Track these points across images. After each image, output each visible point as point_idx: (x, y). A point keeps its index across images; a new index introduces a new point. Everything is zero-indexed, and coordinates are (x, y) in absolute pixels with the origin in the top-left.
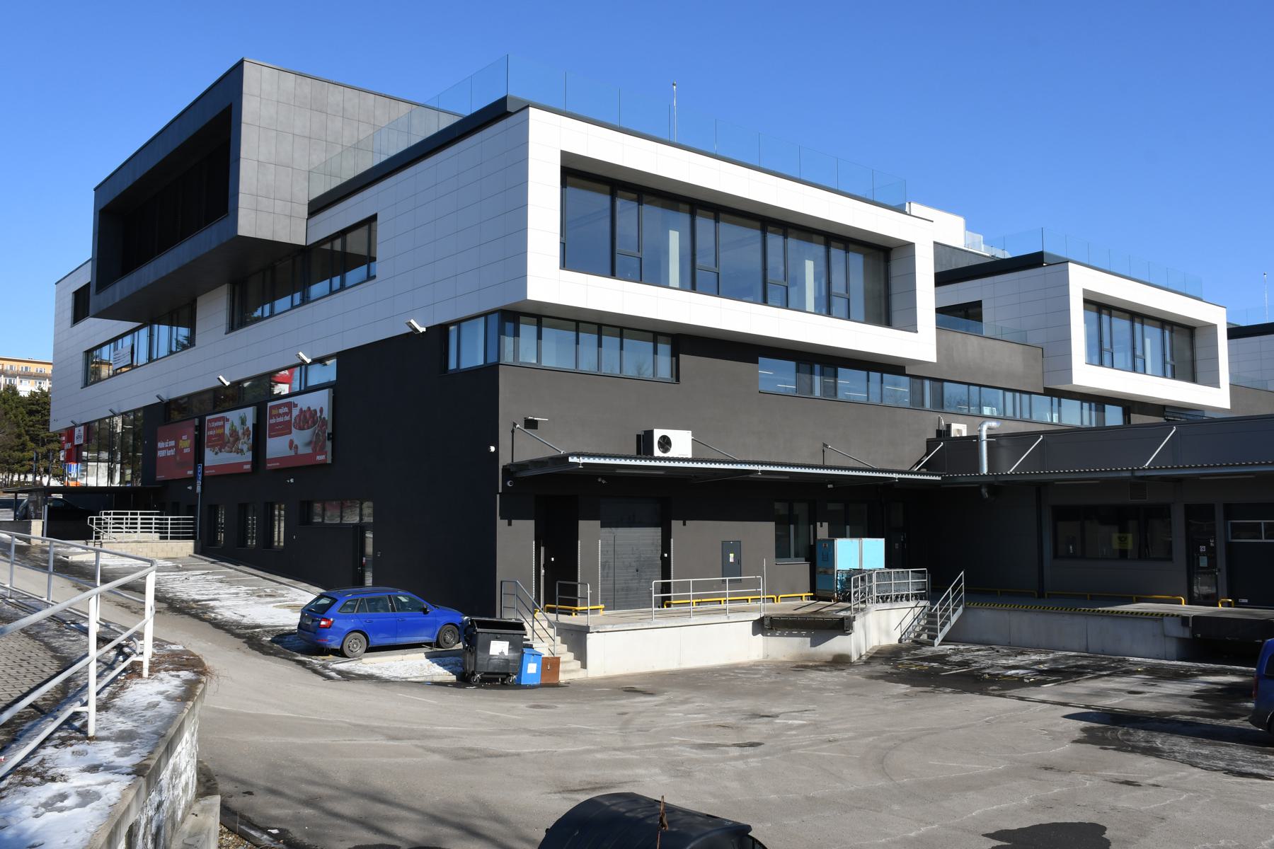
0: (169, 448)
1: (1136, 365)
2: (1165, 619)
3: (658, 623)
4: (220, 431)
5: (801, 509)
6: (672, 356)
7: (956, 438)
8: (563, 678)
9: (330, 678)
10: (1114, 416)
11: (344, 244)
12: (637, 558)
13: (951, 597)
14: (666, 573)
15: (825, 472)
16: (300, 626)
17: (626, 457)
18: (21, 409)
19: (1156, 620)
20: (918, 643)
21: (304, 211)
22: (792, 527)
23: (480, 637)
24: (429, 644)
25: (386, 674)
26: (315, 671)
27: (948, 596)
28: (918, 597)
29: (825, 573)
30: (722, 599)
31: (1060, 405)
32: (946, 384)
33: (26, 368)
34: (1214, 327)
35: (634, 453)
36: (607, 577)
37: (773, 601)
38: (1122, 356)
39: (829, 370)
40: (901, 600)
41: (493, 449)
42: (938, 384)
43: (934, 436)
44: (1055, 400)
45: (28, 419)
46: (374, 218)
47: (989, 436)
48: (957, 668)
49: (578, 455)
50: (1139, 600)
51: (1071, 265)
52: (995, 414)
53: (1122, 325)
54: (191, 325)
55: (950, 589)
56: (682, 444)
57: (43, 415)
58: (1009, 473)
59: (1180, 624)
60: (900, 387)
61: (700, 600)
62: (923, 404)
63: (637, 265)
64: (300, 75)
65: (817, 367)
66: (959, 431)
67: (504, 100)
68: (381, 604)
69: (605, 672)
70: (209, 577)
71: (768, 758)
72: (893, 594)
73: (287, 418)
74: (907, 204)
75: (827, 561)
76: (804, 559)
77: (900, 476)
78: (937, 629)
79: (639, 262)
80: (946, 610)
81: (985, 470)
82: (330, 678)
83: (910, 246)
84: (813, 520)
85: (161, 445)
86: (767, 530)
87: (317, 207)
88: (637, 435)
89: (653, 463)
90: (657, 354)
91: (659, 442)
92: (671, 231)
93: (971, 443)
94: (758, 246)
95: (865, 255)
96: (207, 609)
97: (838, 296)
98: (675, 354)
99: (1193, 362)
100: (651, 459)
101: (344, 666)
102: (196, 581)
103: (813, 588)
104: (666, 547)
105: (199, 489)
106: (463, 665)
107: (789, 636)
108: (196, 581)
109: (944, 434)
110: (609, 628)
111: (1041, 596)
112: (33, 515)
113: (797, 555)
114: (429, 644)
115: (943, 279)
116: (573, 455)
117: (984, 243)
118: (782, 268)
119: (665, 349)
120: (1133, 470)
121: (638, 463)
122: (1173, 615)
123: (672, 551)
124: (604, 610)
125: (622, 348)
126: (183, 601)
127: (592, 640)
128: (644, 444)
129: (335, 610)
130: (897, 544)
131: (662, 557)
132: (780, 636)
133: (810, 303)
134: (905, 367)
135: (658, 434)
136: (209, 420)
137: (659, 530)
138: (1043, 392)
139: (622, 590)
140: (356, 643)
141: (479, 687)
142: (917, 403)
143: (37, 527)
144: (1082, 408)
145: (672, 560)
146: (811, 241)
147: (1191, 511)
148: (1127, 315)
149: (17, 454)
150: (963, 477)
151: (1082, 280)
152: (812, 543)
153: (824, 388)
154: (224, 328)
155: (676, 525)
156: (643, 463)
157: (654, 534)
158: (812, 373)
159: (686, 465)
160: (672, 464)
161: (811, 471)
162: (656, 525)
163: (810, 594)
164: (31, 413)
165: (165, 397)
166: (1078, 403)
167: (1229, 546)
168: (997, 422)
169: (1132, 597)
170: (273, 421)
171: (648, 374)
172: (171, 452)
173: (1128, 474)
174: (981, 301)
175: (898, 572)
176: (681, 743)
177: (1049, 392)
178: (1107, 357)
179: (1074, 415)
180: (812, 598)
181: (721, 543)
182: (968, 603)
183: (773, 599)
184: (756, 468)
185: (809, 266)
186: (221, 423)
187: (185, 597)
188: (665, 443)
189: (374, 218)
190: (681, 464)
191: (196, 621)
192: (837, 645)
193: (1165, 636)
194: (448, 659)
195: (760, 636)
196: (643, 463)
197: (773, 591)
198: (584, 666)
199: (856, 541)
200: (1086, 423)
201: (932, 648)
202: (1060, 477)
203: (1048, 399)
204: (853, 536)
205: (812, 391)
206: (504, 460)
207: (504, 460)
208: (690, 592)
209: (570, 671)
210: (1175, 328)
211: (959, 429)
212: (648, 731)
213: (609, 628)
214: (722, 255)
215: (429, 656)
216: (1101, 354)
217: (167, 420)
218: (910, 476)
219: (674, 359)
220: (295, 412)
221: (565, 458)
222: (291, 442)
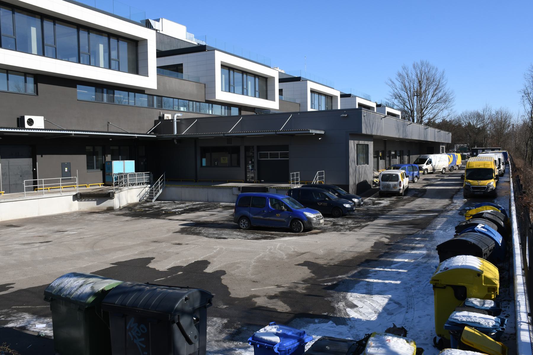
1: (244, 92)
2: (233, 188)
3: (27, 198)
5: (99, 149)
6: (34, 84)
7: (166, 120)
10: (235, 112)
12: (21, 171)
13: (159, 183)
14: (35, 176)
15: (109, 134)
17: (12, 128)
19: (230, 189)
20: (147, 201)
22: (95, 157)
27: (158, 183)
28: (147, 183)
29: (109, 175)
30: (75, 186)
31: (212, 107)
32: (163, 98)
34: (273, 78)
35: (16, 126)
36: (6, 179)
37: (86, 187)
38: (239, 88)
40: (140, 185)
42: (160, 98)
43: (158, 119)
44: (210, 105)
47: (177, 120)
48: (155, 210)
50: (229, 182)
51: (216, 51)
52: (186, 110)
53: (238, 76)
55: (159, 179)
58: (182, 134)
59: (238, 190)
60: (143, 99)
61: (51, 188)
62: (153, 106)
63: (13, 42)
65: (105, 90)
66: (168, 117)
69: (2, 219)
71: (50, 246)
72: (137, 182)
74: (161, 19)
75: (110, 170)
76: (100, 169)
77: (138, 135)
78: (153, 195)
79: (15, 40)
80: (157, 188)
81: (176, 133)
83: (146, 41)
84: (104, 154)
86: (83, 158)
88: (17, 118)
89: (25, 131)
90: (26, 83)
91: (27, 121)
92: (32, 27)
93: (171, 122)
94: (76, 37)
95: (128, 43)
97: (114, 60)
98: (36, 83)
99: (267, 91)
103: (104, 181)
104: (34, 166)
107: (88, 201)
109: (161, 118)
111: (196, 181)
113: (97, 168)
115: (160, 54)
117: (195, 38)
118: (87, 47)
119: (30, 80)
120: (223, 133)
121: (18, 131)
122: (236, 187)
123: (37, 168)
124: (4, 193)
125: (8, 79)
128: (20, 123)
130: (142, 163)
131: (33, 170)
132: (84, 201)
133: (102, 62)
134: (145, 91)
135: (27, 118)
137: (31, 159)
138: (205, 102)
139: (14, 184)
142: (151, 105)
144: (222, 108)
145: (37, 171)
146: (102, 35)
147: (247, 149)
148: (241, 72)
150: (166, 136)
151: (220, 58)
152: (104, 163)
155: (38, 157)
156: (21, 131)
157: (29, 161)
158: (103, 92)
159: (42, 131)
160: (33, 131)
161: (97, 134)
162: (30, 157)
163: (102, 184)
166: (220, 106)
167: (259, 161)
168: (181, 114)
169: (227, 181)
171: (22, 91)
173: (222, 135)
174: (182, 64)
175: (139, 174)
176: (16, 244)
177: (207, 102)
178: (232, 88)
179: (218, 111)
180: (104, 185)
181: (61, 164)
182: (166, 185)
183: (86, 186)
184: (71, 132)
185: (101, 47)
188: (31, 122)
190: (40, 131)
192: (107, 204)
193: (233, 194)
195: (76, 201)
196: (21, 131)
197: (83, 182)
199: (122, 162)
200: (223, 114)
201: (151, 203)
202: (204, 136)
203: (207, 104)
204: (122, 160)
205: (103, 100)
208: (43, 186)
210: (260, 77)
211: (168, 116)
212: (5, 240)
213: (2, 201)
214: (57, 40)
216: (229, 88)
218: (146, 136)
219: (35, 85)
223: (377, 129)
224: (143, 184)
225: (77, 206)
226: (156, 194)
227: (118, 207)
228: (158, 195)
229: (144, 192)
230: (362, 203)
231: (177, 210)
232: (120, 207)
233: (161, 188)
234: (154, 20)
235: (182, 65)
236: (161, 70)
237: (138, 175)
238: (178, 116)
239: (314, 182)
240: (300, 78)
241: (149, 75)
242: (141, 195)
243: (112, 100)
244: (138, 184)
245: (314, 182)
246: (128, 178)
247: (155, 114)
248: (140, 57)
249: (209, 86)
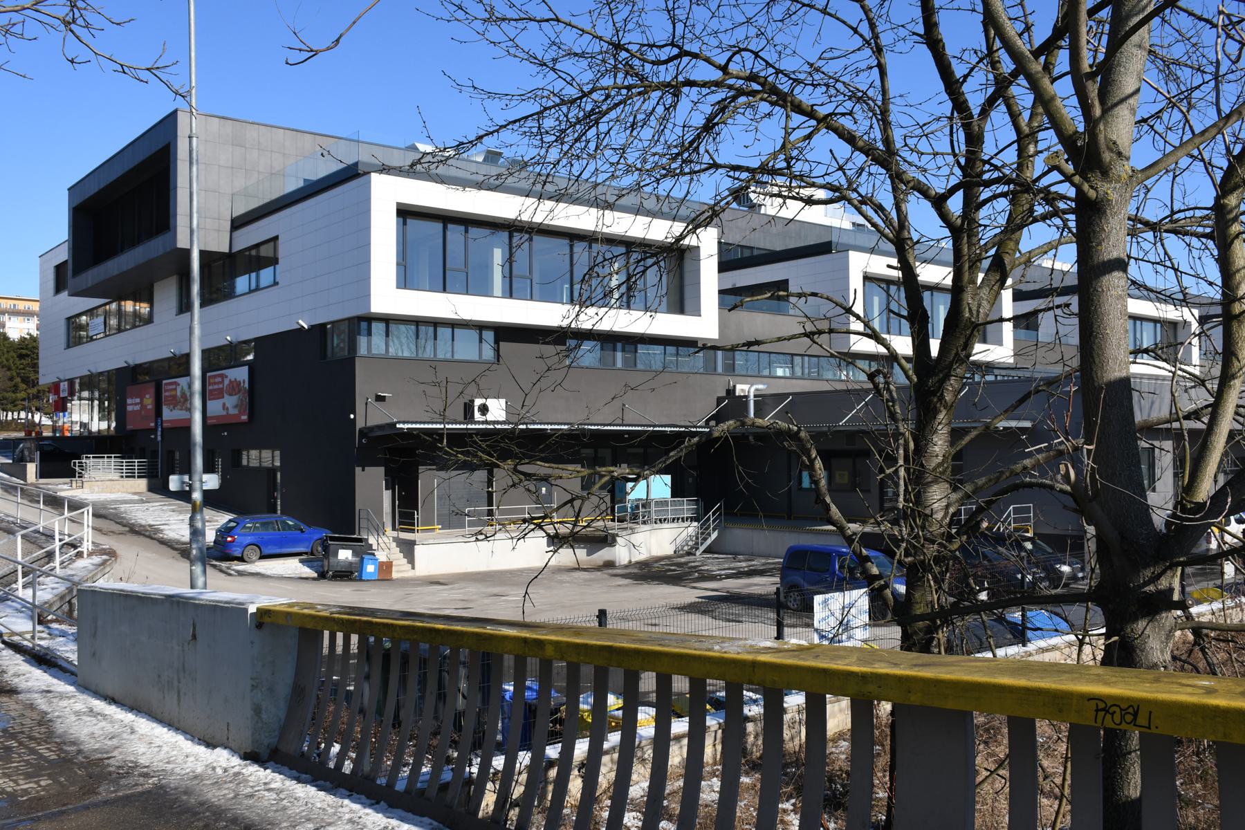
0: (136, 404)
4: (173, 393)
8: (395, 575)
9: (230, 575)
11: (258, 252)
14: (490, 503)
16: (215, 542)
18: (12, 353)
21: (228, 225)
23: (331, 547)
24: (306, 553)
25: (268, 572)
26: (221, 571)
27: (708, 519)
28: (692, 519)
33: (14, 305)
39: (629, 347)
41: (352, 416)
45: (18, 363)
46: (276, 238)
47: (755, 396)
49: (404, 423)
52: (788, 374)
54: (151, 302)
56: (497, 410)
57: (33, 359)
62: (715, 369)
64: (223, 118)
65: (619, 345)
66: (742, 390)
67: (356, 164)
68: (271, 526)
70: (165, 508)
73: (221, 386)
80: (707, 529)
82: (230, 575)
85: (129, 401)
87: (238, 223)
96: (158, 531)
98: (497, 341)
100: (472, 423)
101: (241, 567)
102: (154, 511)
104: (490, 484)
105: (159, 438)
106: (322, 566)
108: (154, 511)
109: (731, 392)
110: (431, 541)
111: (789, 518)
112: (28, 459)
114: (306, 553)
116: (399, 422)
126: (141, 526)
127: (418, 550)
129: (238, 530)
136: (166, 384)
140: (252, 553)
141: (330, 580)
143: (31, 469)
149: (10, 395)
153: (625, 361)
154: (174, 310)
158: (615, 350)
164: (21, 357)
165: (132, 363)
170: (211, 388)
172: (137, 408)
186: (174, 387)
187: (143, 522)
188: (484, 409)
189: (276, 238)
191: (148, 540)
192: (604, 554)
194: (315, 564)
198: (413, 568)
205: (614, 363)
206: (360, 424)
207: (360, 424)
209: (401, 569)
211: (741, 389)
213: (431, 541)
215: (302, 561)
217: (134, 381)
220: (226, 382)
221: (394, 424)
222: (224, 405)
224: (683, 521)
226: (705, 539)
227: (625, 561)
228: (709, 542)
229: (684, 535)
230: (1080, 575)
231: (723, 572)
232: (630, 562)
233: (714, 530)
236: (732, 299)
237: (673, 504)
238: (757, 390)
239: (999, 528)
240: (830, 243)
241: (702, 313)
242: (678, 541)
243: (631, 364)
244: (674, 519)
245: (999, 528)
246: (653, 508)
248: (687, 281)
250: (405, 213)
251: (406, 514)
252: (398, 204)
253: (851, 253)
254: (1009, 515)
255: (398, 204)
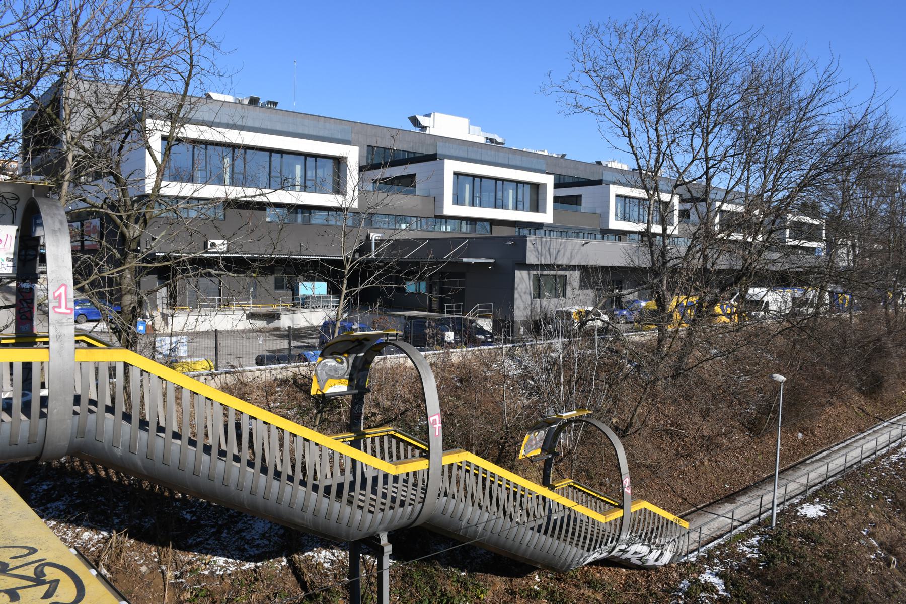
47: (376, 240)
99: (537, 200)
192: (275, 324)
205: (296, 221)
223: (571, 257)
225: (245, 324)
234: (425, 116)
235: (581, 196)
240: (435, 155)
247: (361, 233)
249: (438, 199)
250: (456, 174)
251: (173, 301)
252: (346, 158)
253: (446, 161)
254: (476, 308)
255: (346, 158)
